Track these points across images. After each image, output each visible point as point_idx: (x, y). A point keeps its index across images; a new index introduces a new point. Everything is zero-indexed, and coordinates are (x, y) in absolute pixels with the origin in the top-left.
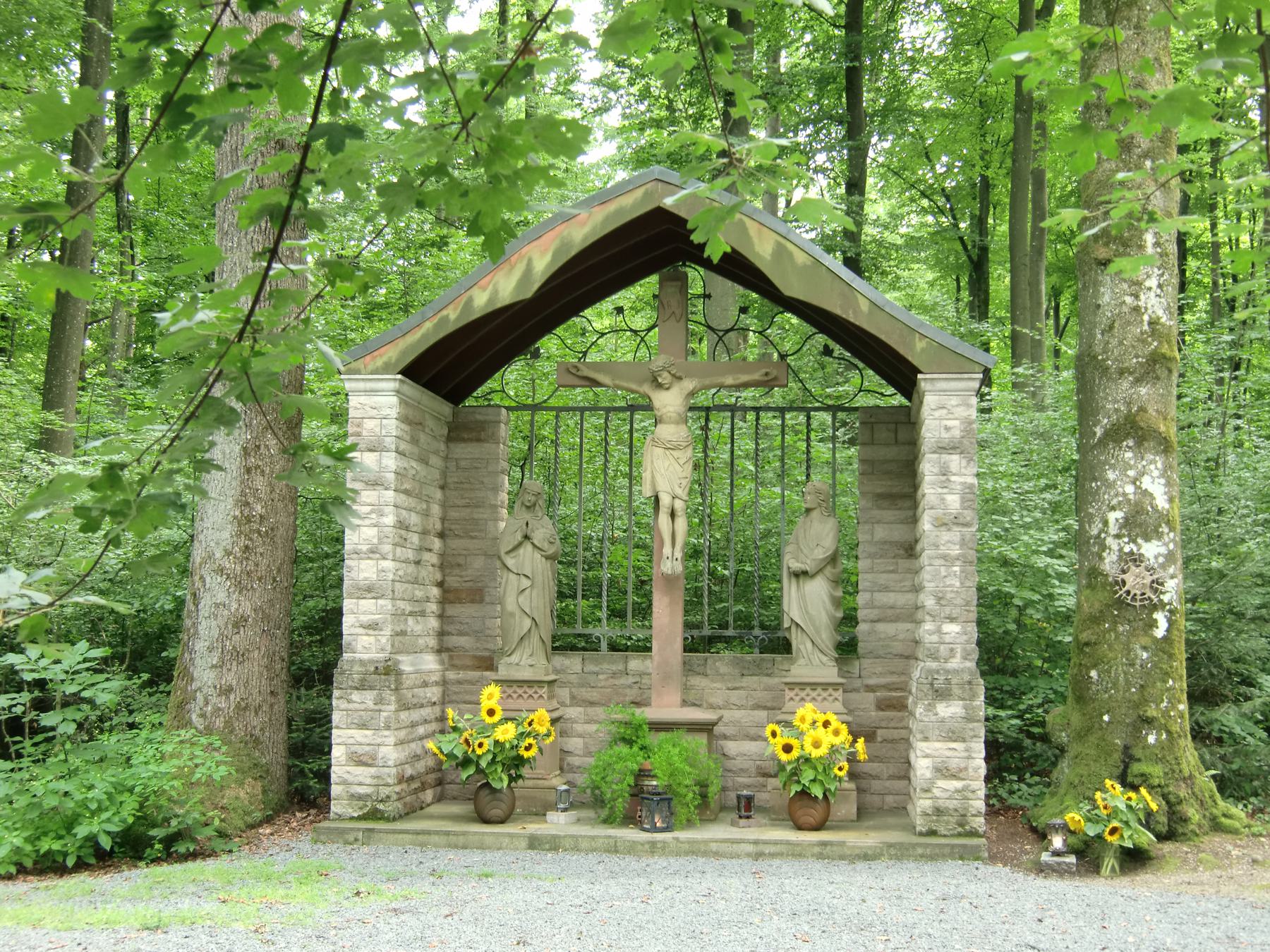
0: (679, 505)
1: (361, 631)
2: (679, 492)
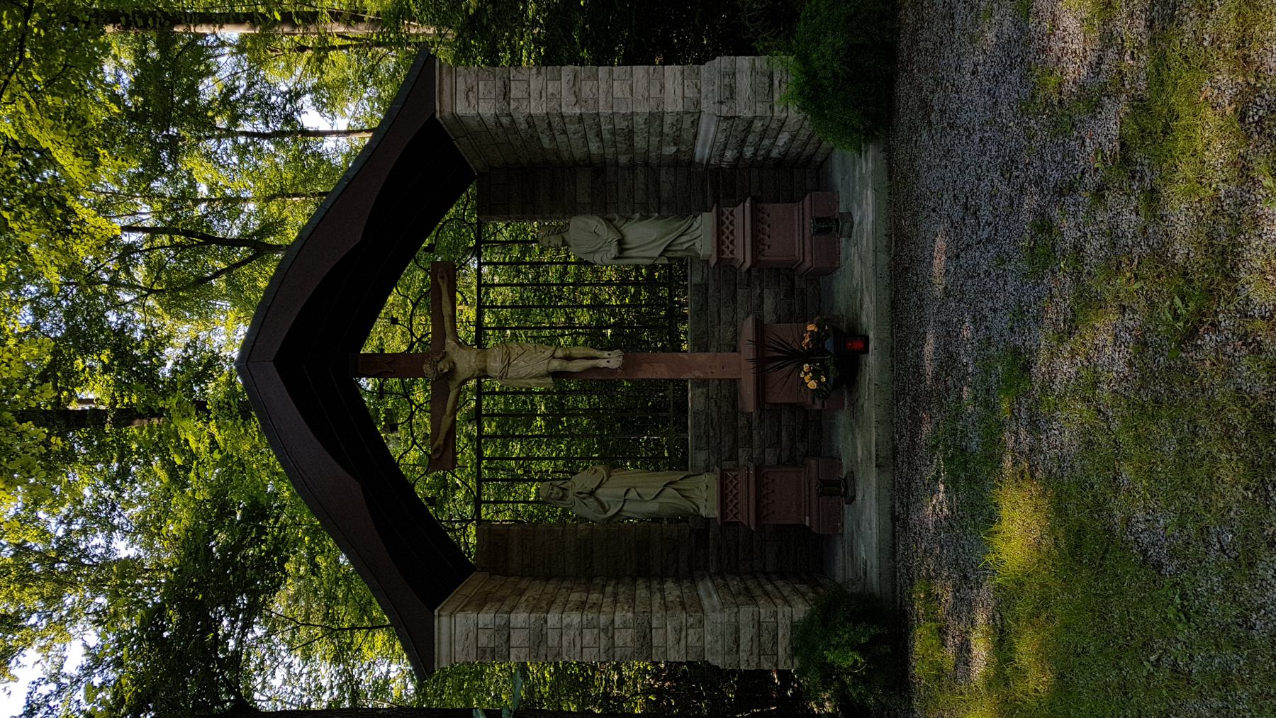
1: (683, 642)
2: (548, 353)
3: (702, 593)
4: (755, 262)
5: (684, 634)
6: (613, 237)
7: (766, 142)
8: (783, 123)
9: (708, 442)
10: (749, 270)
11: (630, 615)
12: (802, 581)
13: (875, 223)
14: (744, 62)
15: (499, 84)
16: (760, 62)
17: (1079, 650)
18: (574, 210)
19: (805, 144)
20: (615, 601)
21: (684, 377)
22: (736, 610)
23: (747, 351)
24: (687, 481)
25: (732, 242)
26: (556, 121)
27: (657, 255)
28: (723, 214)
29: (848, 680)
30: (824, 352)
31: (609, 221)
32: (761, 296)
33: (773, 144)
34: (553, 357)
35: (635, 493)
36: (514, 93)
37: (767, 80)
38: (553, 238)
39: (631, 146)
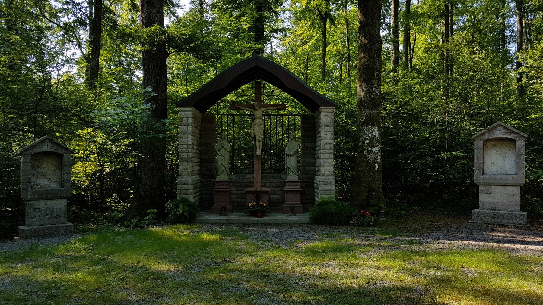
0: (260, 139)
3: (196, 176)
6: (292, 153)
12: (199, 203)
13: (290, 220)
14: (334, 187)
20: (194, 153)
23: (259, 189)
29: (175, 210)
30: (258, 207)
32: (278, 194)
35: (223, 159)
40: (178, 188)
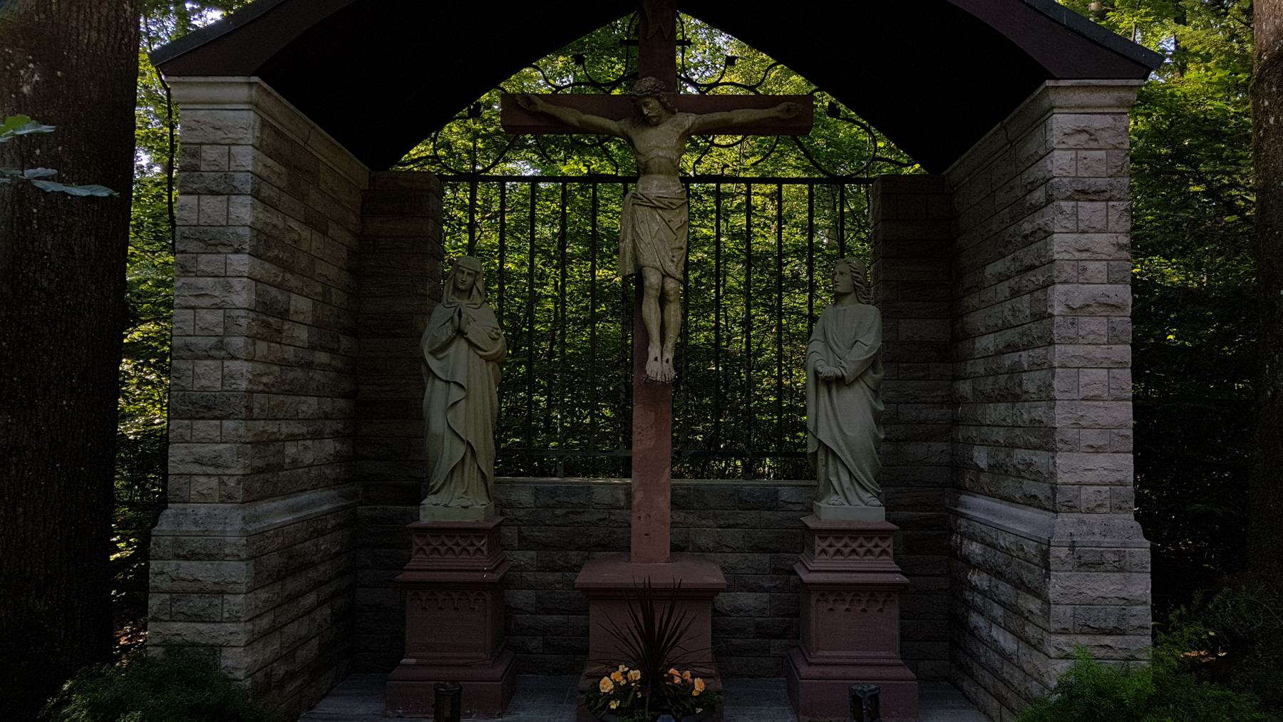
0: (671, 285)
1: (197, 469)
2: (671, 268)
4: (809, 588)
5: (211, 470)
6: (849, 371)
7: (998, 611)
8: (1037, 646)
9: (546, 506)
10: (793, 572)
11: (244, 385)
14: (1141, 586)
15: (1102, 183)
16: (1143, 615)
17: (1244, 18)
18: (888, 315)
19: (994, 672)
21: (634, 473)
22: (243, 555)
24: (476, 475)
25: (838, 552)
26: (1038, 277)
27: (820, 436)
28: (884, 539)
31: (872, 364)
33: (994, 621)
34: (665, 275)
35: (460, 400)
36: (1086, 207)
37: (1112, 625)
38: (847, 278)
39: (989, 399)
40: (154, 581)
